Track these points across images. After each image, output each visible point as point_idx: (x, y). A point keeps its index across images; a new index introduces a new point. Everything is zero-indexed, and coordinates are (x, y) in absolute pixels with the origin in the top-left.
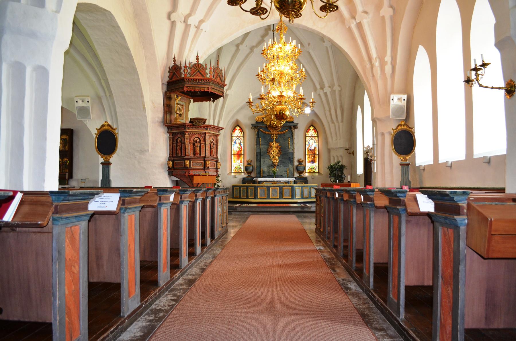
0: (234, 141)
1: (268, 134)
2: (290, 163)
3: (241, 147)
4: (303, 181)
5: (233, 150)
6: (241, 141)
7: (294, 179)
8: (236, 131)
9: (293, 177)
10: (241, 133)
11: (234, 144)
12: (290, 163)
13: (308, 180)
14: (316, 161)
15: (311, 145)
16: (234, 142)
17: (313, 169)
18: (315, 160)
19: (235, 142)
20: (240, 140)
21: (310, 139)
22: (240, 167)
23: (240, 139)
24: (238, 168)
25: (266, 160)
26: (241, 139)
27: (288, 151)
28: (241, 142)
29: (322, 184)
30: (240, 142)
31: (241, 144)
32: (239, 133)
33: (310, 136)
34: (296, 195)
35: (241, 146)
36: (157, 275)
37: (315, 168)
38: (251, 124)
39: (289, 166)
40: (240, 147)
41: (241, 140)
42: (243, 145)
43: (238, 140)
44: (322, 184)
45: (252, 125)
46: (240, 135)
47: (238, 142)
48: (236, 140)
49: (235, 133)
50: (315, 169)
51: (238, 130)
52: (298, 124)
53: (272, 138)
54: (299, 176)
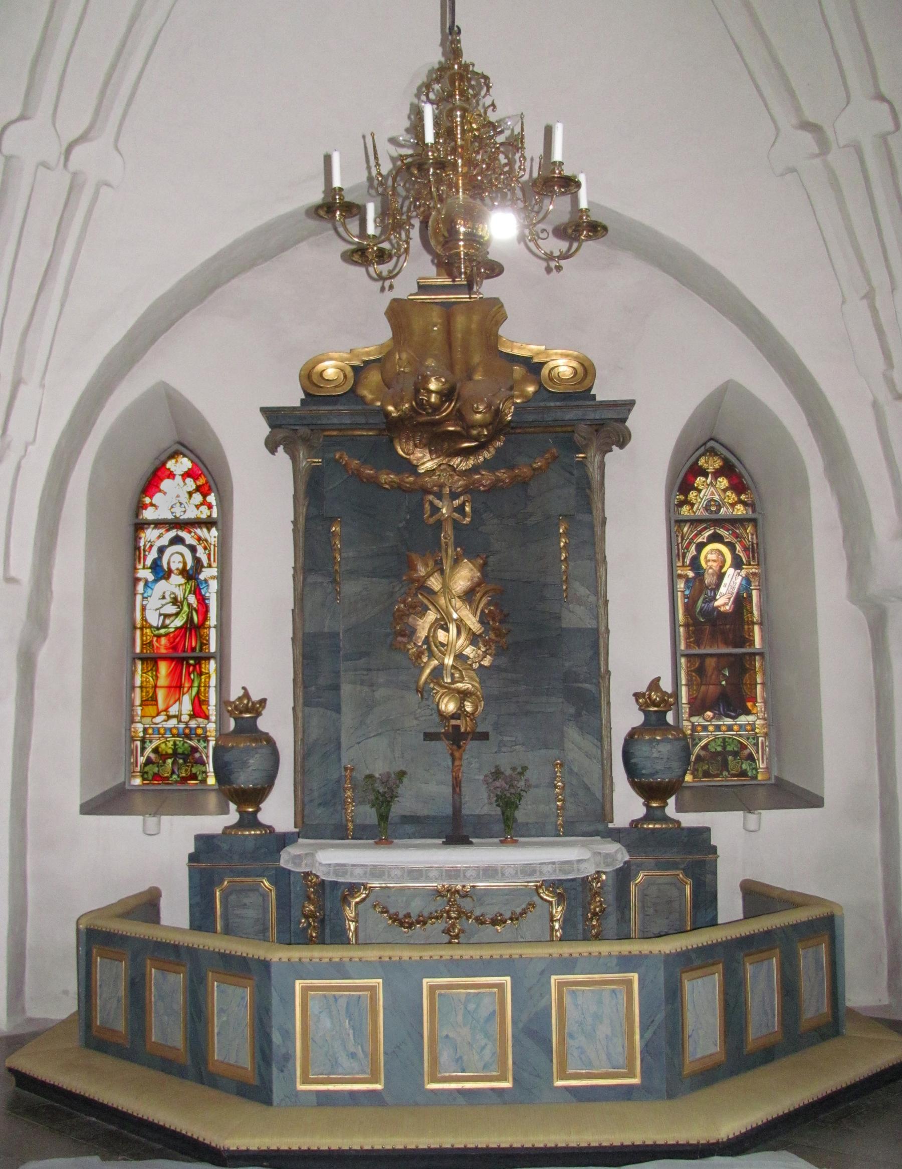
0: (153, 555)
1: (399, 488)
2: (578, 715)
3: (202, 601)
4: (676, 858)
5: (144, 618)
6: (201, 553)
7: (617, 853)
8: (166, 484)
9: (600, 827)
10: (198, 498)
11: (151, 577)
12: (578, 715)
13: (714, 850)
14: (754, 700)
15: (709, 579)
16: (149, 562)
17: (735, 754)
18: (746, 690)
19: (156, 567)
20: (193, 549)
21: (702, 538)
22: (194, 750)
23: (194, 542)
24: (175, 754)
25: (381, 693)
26: (199, 539)
27: (559, 618)
28: (197, 561)
29: (488, 739)
30: (190, 563)
31: (202, 577)
32: (184, 498)
33: (700, 521)
34: (689, 1047)
35: (197, 592)
36: (475, 615)
37: (744, 747)
38: (266, 411)
39: (568, 745)
40: (192, 599)
41: (200, 550)
42: (214, 585)
43: (180, 548)
44: (488, 739)
45: (272, 415)
46: (191, 513)
47: (176, 565)
48: (161, 550)
49: (158, 498)
50: (750, 757)
51: (179, 479)
52: (629, 405)
53: (432, 520)
54: (647, 818)
